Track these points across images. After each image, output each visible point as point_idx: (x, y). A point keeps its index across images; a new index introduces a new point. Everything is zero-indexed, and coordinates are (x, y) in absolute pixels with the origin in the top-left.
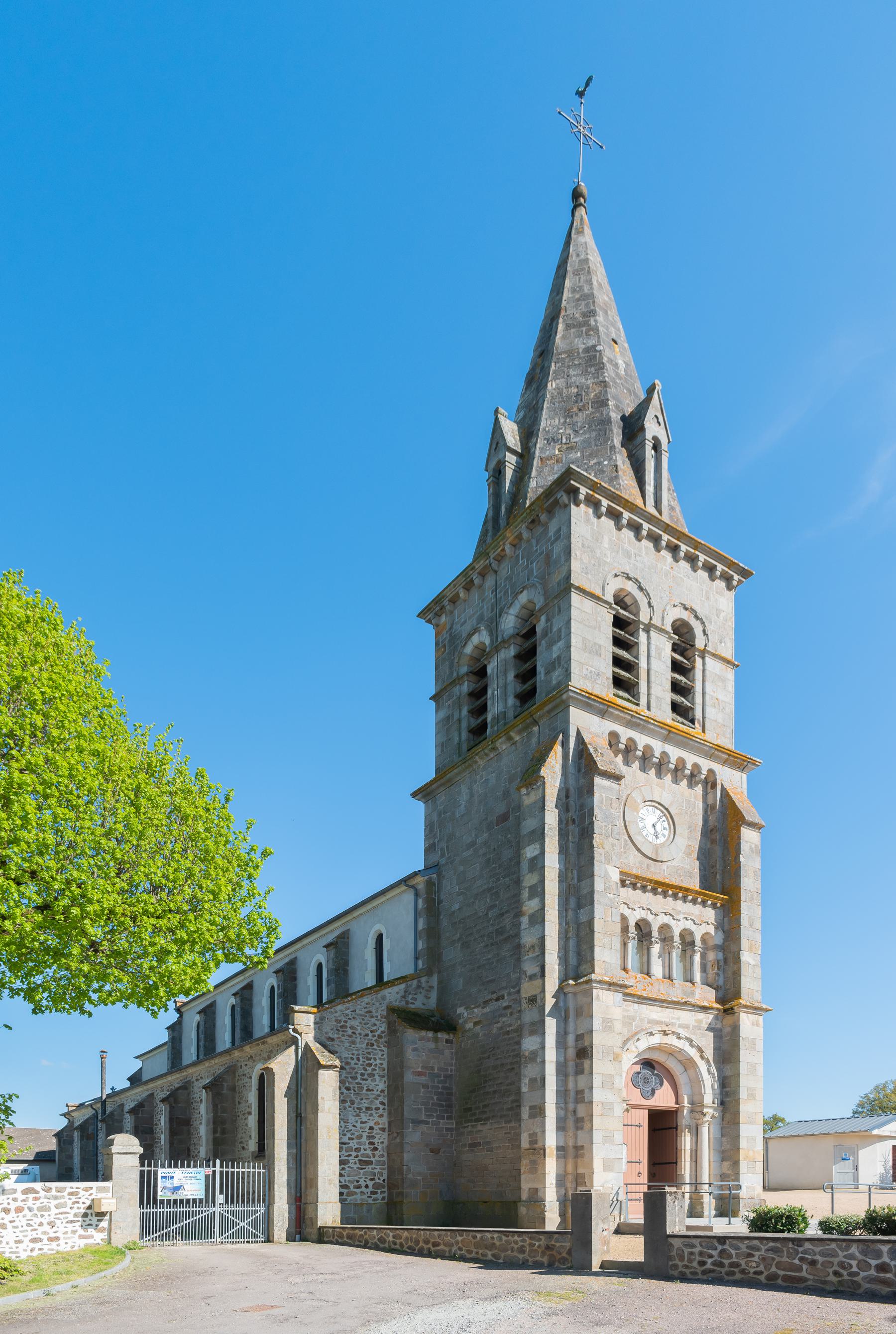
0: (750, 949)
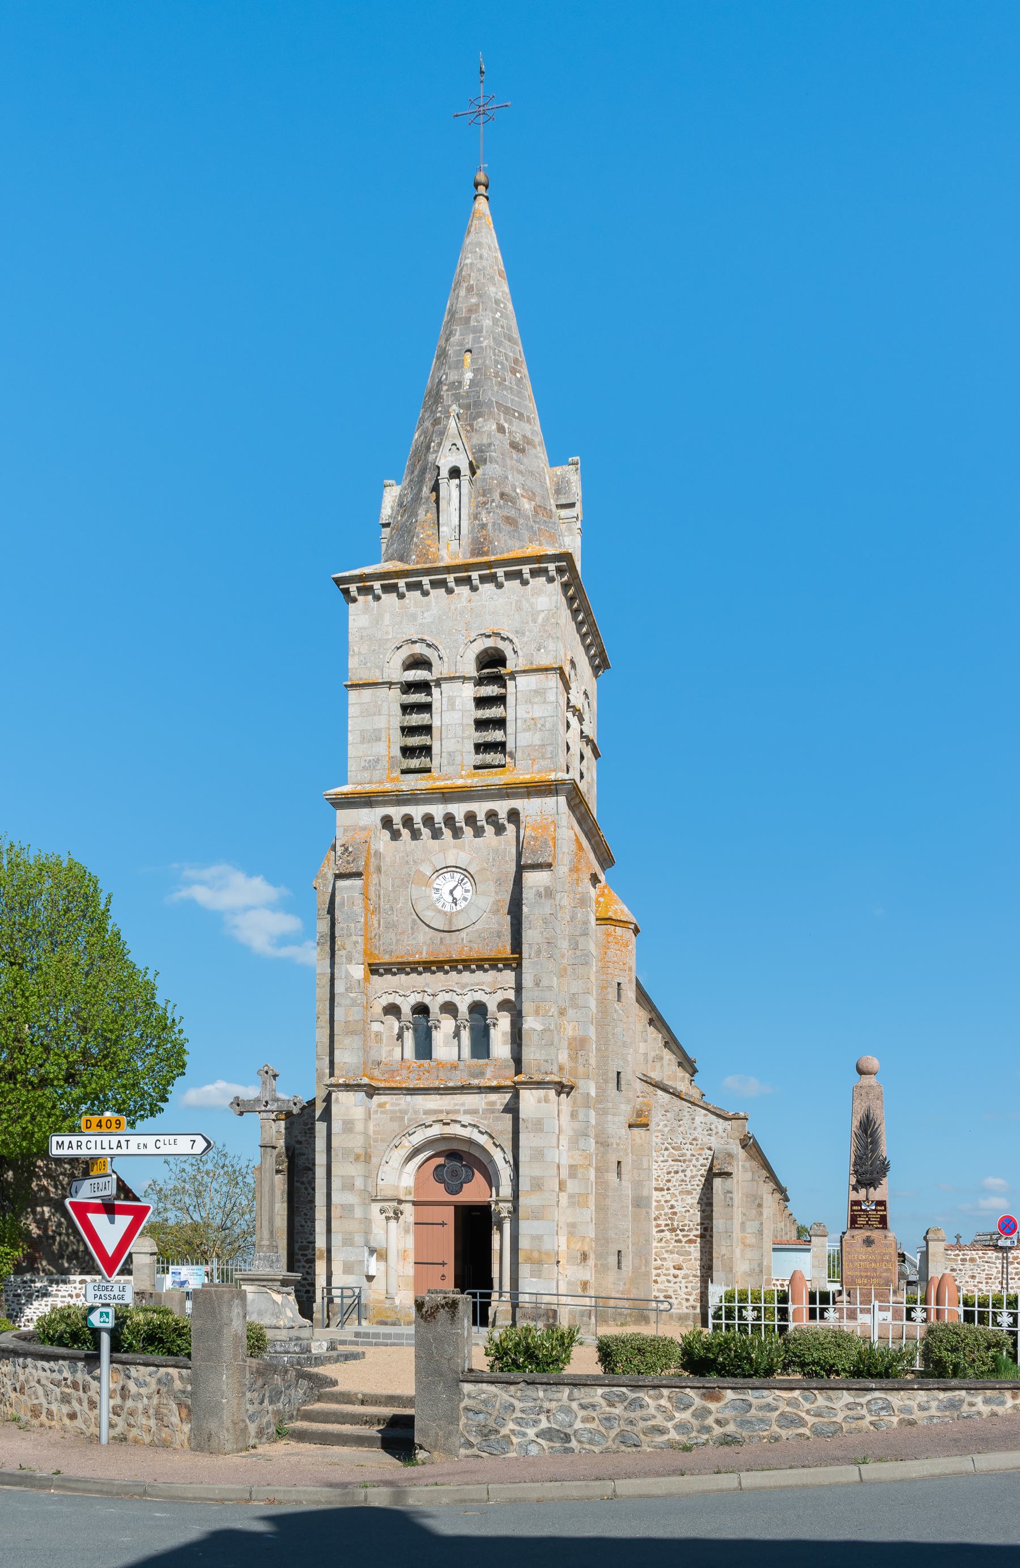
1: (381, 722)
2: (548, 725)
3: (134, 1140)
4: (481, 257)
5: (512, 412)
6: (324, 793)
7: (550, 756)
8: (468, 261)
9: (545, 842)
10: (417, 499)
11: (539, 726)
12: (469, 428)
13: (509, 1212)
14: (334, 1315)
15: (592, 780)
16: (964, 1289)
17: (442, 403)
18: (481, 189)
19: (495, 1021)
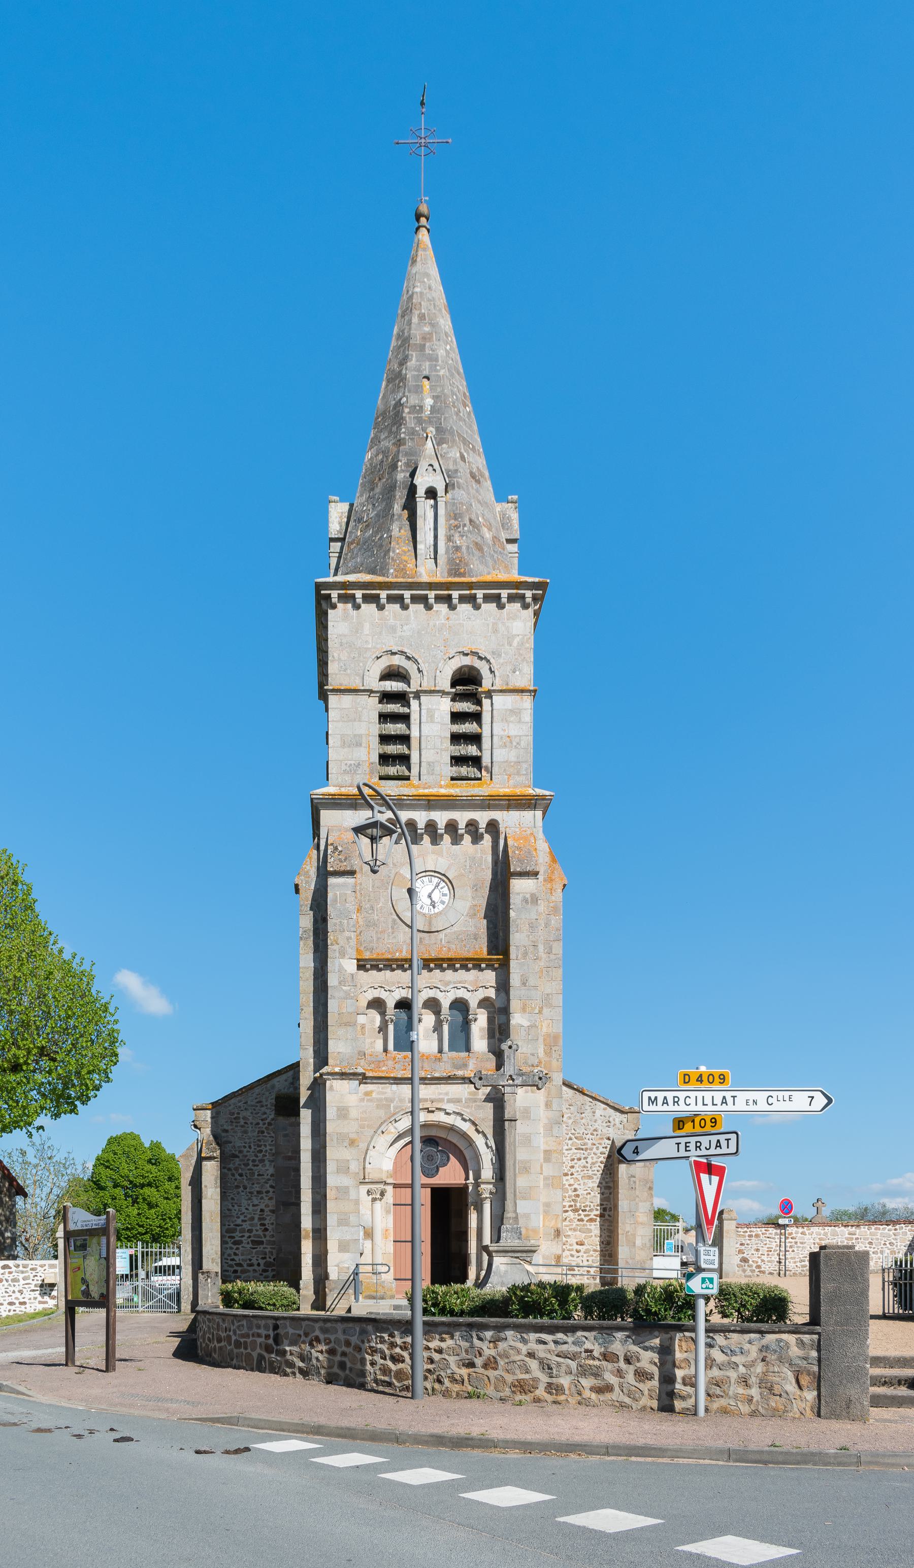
0: (524, 1010)
3: (742, 1097)
4: (430, 288)
6: (311, 793)
7: (524, 772)
10: (386, 515)
11: (514, 744)
13: (491, 1193)
14: (330, 1291)
16: (751, 1260)
17: (405, 424)
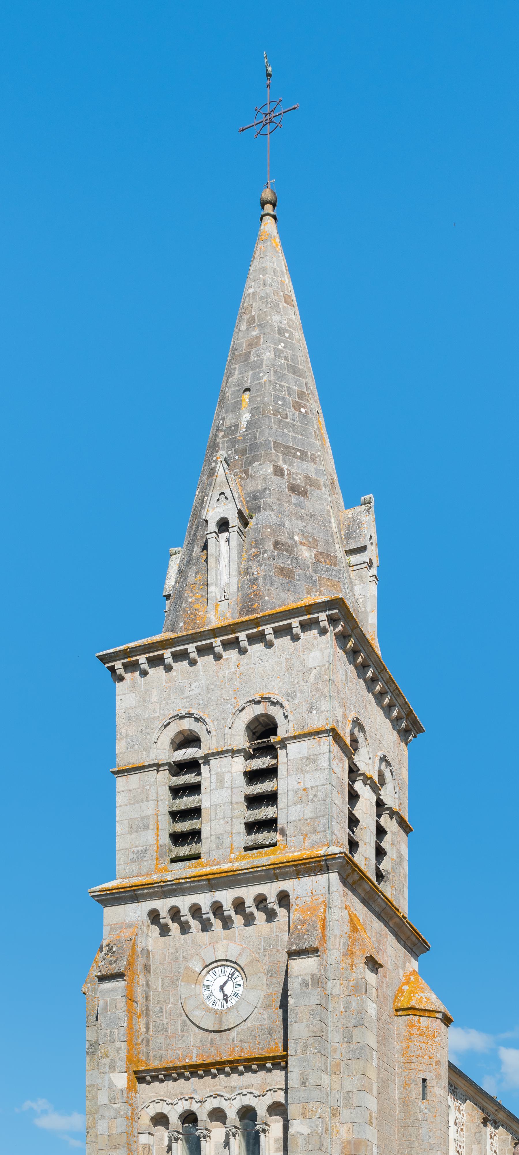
0: (303, 1115)
1: (148, 809)
2: (320, 795)
4: (264, 284)
5: (293, 451)
6: (89, 890)
7: (322, 829)
8: (251, 291)
9: (313, 926)
12: (243, 475)
15: (400, 856)
18: (268, 208)
19: (264, 1126)
